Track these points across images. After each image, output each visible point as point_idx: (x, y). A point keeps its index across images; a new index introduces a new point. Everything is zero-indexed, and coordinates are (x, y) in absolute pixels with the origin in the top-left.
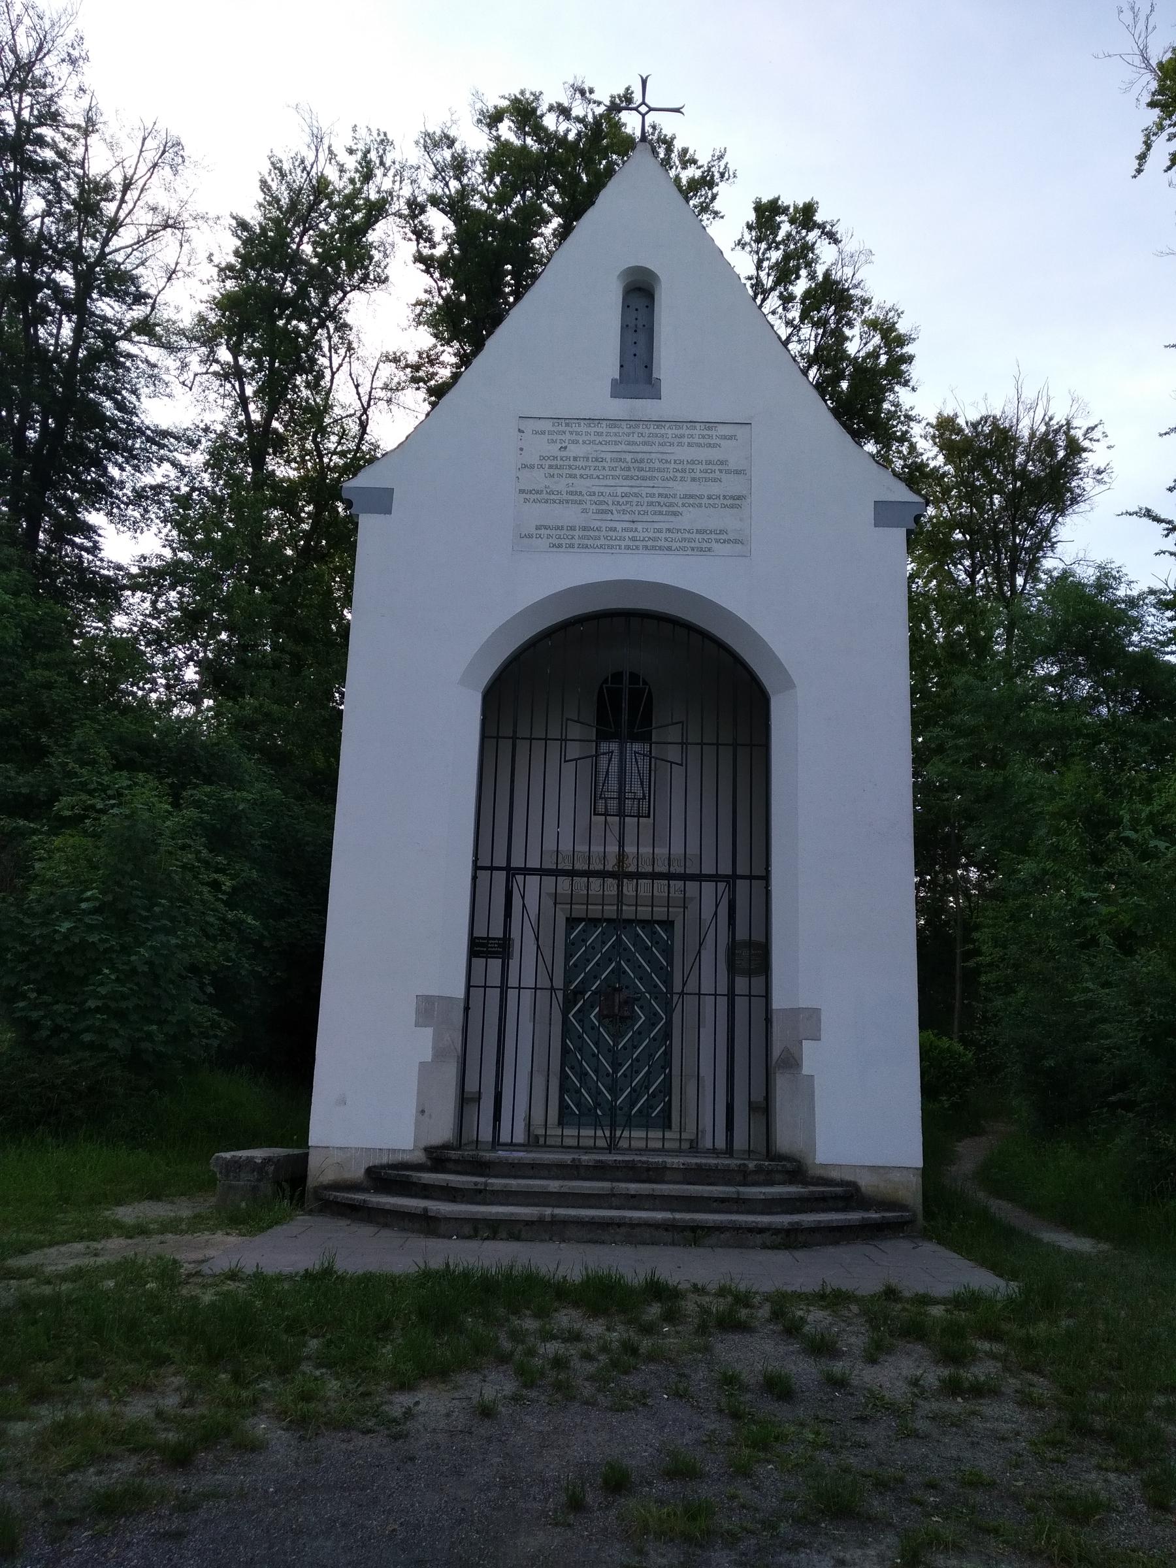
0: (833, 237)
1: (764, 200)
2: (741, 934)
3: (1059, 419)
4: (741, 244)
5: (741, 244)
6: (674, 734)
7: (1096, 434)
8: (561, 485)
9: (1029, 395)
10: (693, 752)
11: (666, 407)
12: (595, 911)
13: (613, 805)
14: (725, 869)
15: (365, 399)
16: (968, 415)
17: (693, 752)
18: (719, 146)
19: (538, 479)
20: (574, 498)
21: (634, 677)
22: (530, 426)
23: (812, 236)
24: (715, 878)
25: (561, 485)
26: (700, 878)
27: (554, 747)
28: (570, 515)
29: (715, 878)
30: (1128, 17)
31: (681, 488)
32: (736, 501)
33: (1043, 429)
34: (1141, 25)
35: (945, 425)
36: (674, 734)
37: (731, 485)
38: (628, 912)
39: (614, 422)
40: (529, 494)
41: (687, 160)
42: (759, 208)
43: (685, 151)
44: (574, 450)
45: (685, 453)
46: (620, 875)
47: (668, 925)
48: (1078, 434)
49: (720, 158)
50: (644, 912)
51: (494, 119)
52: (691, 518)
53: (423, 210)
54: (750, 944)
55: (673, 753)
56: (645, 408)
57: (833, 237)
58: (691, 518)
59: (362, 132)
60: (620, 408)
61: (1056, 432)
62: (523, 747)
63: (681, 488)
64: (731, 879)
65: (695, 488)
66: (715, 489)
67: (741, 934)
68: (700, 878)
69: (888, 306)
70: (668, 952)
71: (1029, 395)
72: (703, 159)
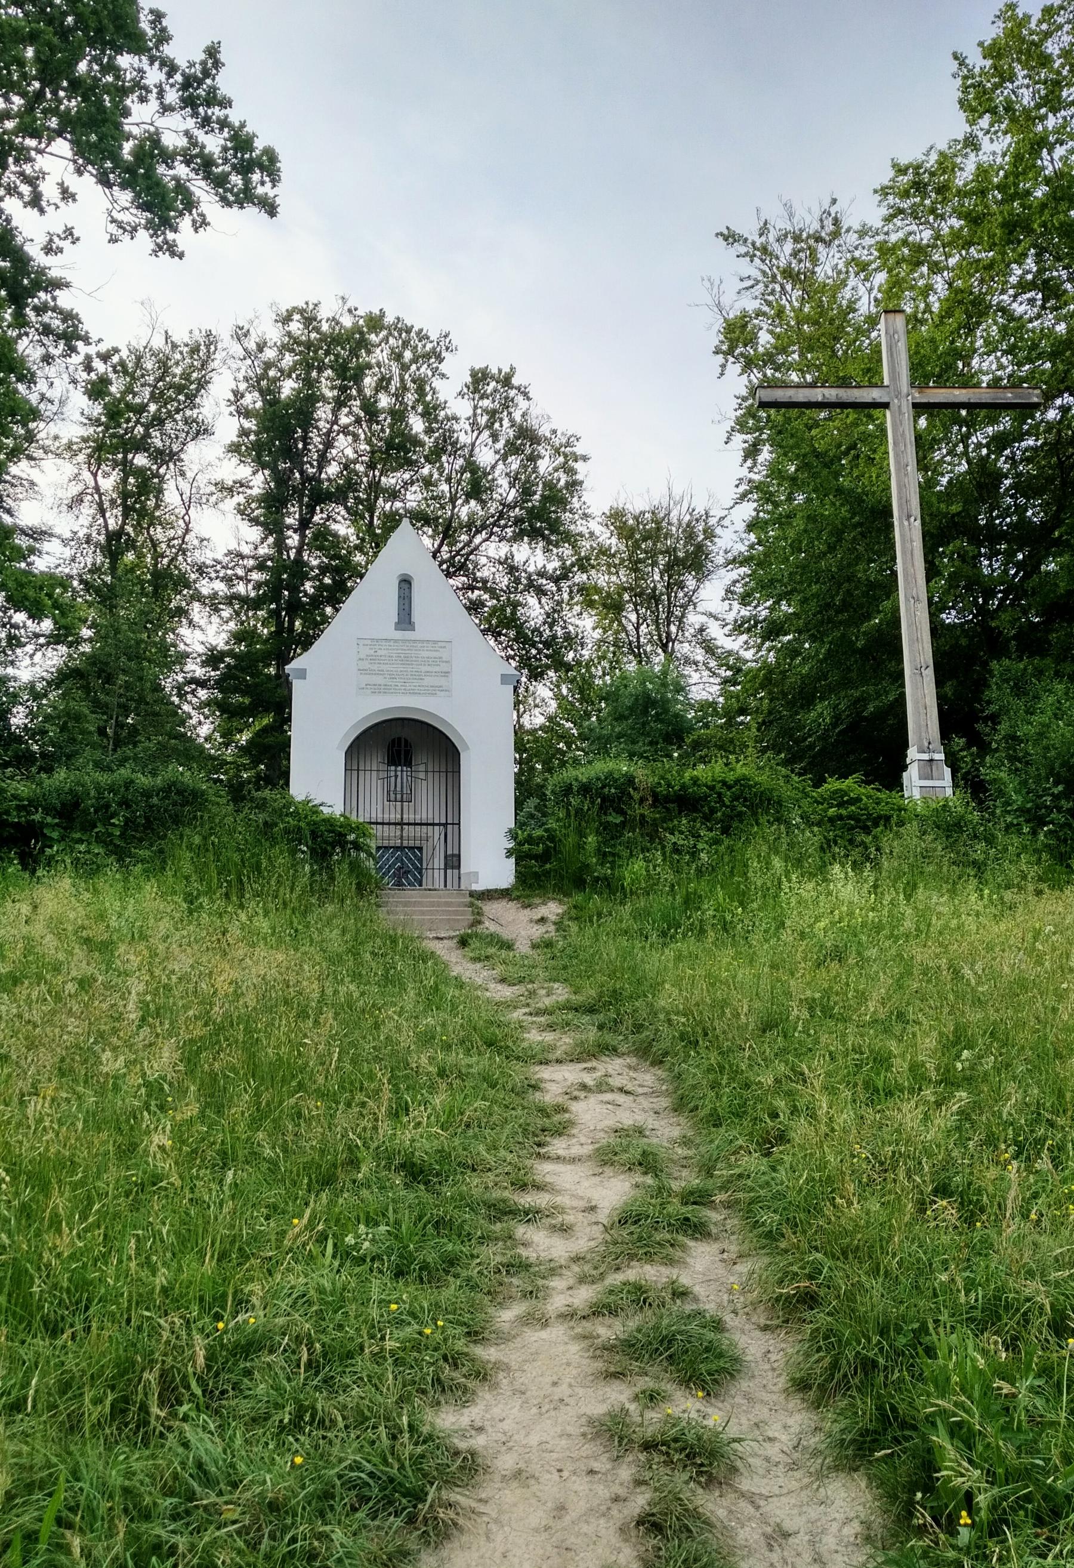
0: (526, 396)
1: (477, 368)
2: (449, 852)
3: (700, 510)
4: (461, 394)
5: (461, 394)
6: (422, 768)
7: (726, 522)
8: (375, 667)
9: (677, 493)
10: (430, 775)
11: (418, 634)
12: (386, 843)
13: (399, 797)
14: (443, 821)
15: (186, 500)
16: (637, 504)
17: (430, 775)
18: (445, 330)
19: (366, 665)
20: (380, 673)
21: (406, 741)
22: (361, 642)
23: (512, 393)
24: (439, 824)
25: (375, 667)
26: (433, 824)
27: (374, 774)
28: (379, 680)
29: (439, 824)
30: (707, 284)
31: (424, 669)
32: (446, 674)
33: (688, 517)
34: (715, 290)
35: (616, 518)
36: (422, 768)
37: (444, 667)
38: (405, 843)
39: (396, 641)
40: (362, 671)
41: (423, 336)
42: (474, 374)
43: (421, 330)
44: (380, 653)
45: (425, 654)
46: (401, 824)
47: (420, 849)
48: (712, 521)
49: (446, 336)
50: (411, 844)
51: (286, 319)
52: (429, 681)
53: (242, 396)
54: (453, 855)
55: (422, 775)
56: (408, 635)
57: (526, 396)
58: (429, 681)
59: (196, 333)
60: (399, 635)
61: (697, 520)
62: (361, 773)
63: (424, 669)
64: (445, 825)
65: (429, 669)
66: (437, 669)
67: (449, 852)
68: (433, 824)
69: (570, 433)
70: (420, 860)
71: (677, 493)
72: (434, 337)
